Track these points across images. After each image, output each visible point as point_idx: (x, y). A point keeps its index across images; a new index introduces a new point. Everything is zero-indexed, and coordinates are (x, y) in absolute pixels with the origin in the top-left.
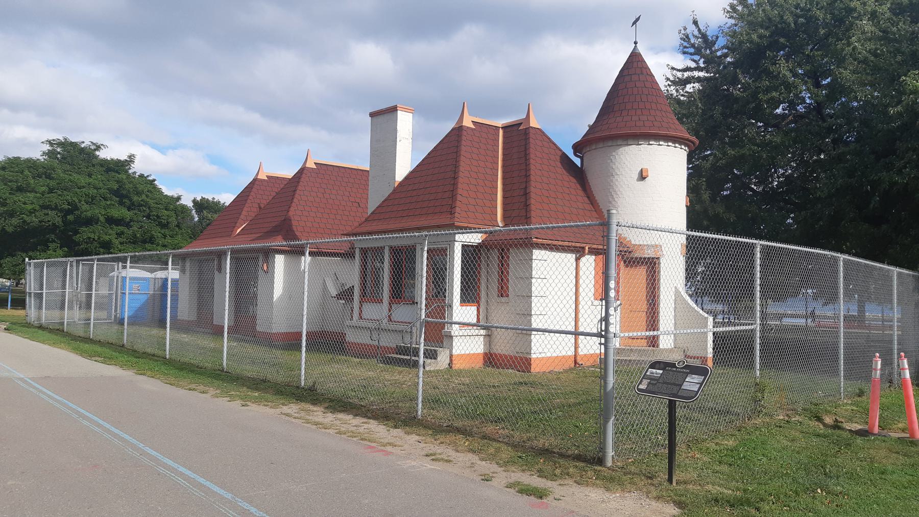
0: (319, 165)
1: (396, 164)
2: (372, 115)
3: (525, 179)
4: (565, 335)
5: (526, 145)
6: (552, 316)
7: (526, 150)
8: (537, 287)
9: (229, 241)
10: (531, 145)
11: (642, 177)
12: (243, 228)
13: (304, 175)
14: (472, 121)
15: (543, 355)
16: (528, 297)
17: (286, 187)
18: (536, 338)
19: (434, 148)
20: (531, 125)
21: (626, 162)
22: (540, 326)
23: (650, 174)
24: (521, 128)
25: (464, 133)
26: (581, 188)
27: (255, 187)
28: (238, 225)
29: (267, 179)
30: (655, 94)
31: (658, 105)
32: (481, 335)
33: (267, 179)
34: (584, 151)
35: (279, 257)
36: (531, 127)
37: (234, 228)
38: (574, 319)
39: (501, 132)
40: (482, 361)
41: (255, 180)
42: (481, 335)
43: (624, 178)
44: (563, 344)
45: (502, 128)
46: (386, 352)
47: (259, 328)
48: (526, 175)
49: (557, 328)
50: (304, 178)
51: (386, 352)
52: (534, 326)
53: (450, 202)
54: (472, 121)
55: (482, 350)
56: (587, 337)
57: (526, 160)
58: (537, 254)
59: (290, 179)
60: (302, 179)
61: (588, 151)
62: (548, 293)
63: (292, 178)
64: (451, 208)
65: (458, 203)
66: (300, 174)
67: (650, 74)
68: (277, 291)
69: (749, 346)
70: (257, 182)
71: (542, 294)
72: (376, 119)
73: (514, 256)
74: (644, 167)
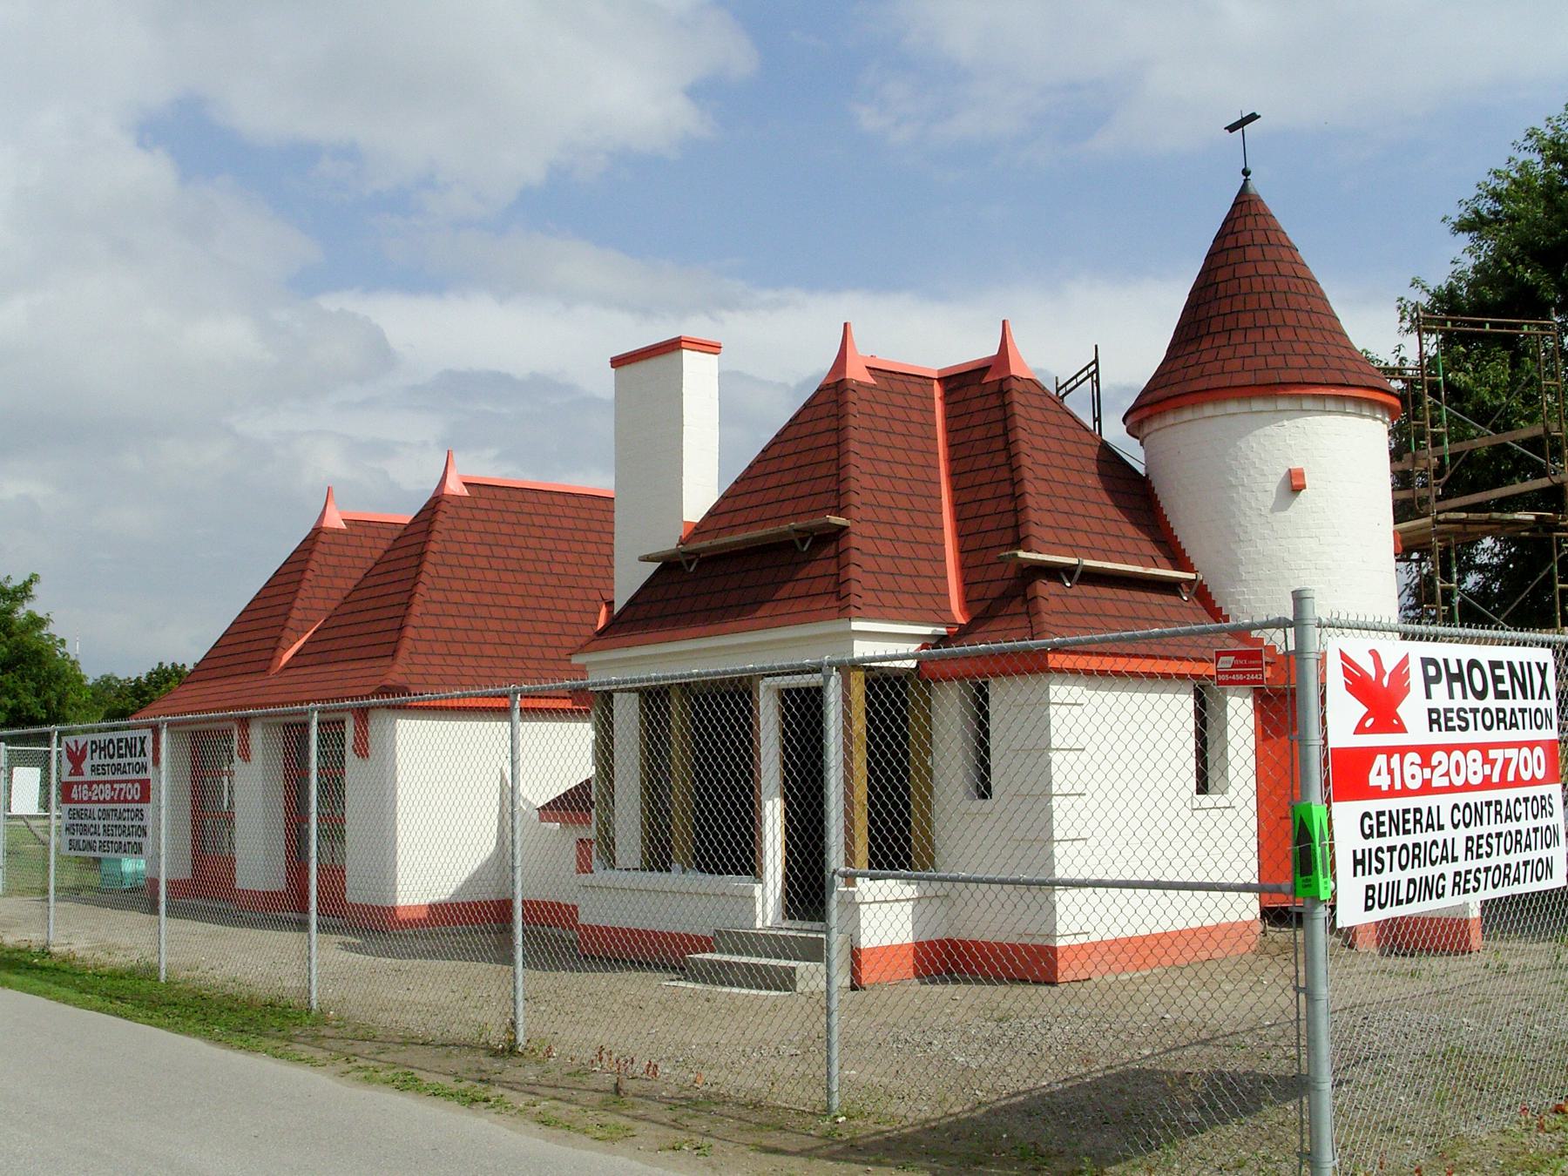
0: (475, 488)
1: (684, 479)
2: (617, 362)
3: (1013, 504)
4: (1204, 893)
5: (1006, 419)
6: (1134, 840)
7: (1006, 432)
8: (1063, 770)
9: (265, 683)
10: (1020, 422)
11: (1294, 485)
12: (300, 650)
13: (440, 516)
14: (867, 367)
15: (1082, 939)
16: (1041, 794)
17: (398, 545)
18: (1062, 897)
19: (777, 435)
20: (1013, 373)
21: (1251, 455)
22: (1073, 874)
23: (1308, 481)
24: (987, 379)
25: (852, 396)
26: (1127, 518)
27: (317, 548)
28: (284, 643)
29: (344, 527)
30: (1303, 290)
31: (1314, 317)
32: (908, 900)
33: (344, 527)
34: (1146, 431)
35: (407, 725)
36: (1014, 377)
37: (275, 649)
38: (1256, 855)
39: (937, 391)
40: (910, 960)
41: (317, 531)
42: (908, 900)
43: (1247, 494)
44: (1101, 910)
45: (939, 380)
46: (686, 947)
47: (351, 897)
48: (1014, 494)
49: (1113, 875)
50: (442, 522)
51: (686, 947)
52: (1059, 873)
53: (833, 569)
54: (867, 367)
55: (911, 934)
56: (1098, 890)
57: (1010, 457)
58: (1059, 691)
59: (407, 527)
60: (438, 526)
61: (1157, 430)
62: (1092, 786)
63: (414, 522)
64: (838, 584)
65: (853, 572)
66: (430, 512)
67: (1287, 244)
68: (491, 810)
69: (1543, 901)
70: (322, 537)
71: (1079, 789)
72: (626, 370)
73: (1004, 696)
74: (1296, 465)
